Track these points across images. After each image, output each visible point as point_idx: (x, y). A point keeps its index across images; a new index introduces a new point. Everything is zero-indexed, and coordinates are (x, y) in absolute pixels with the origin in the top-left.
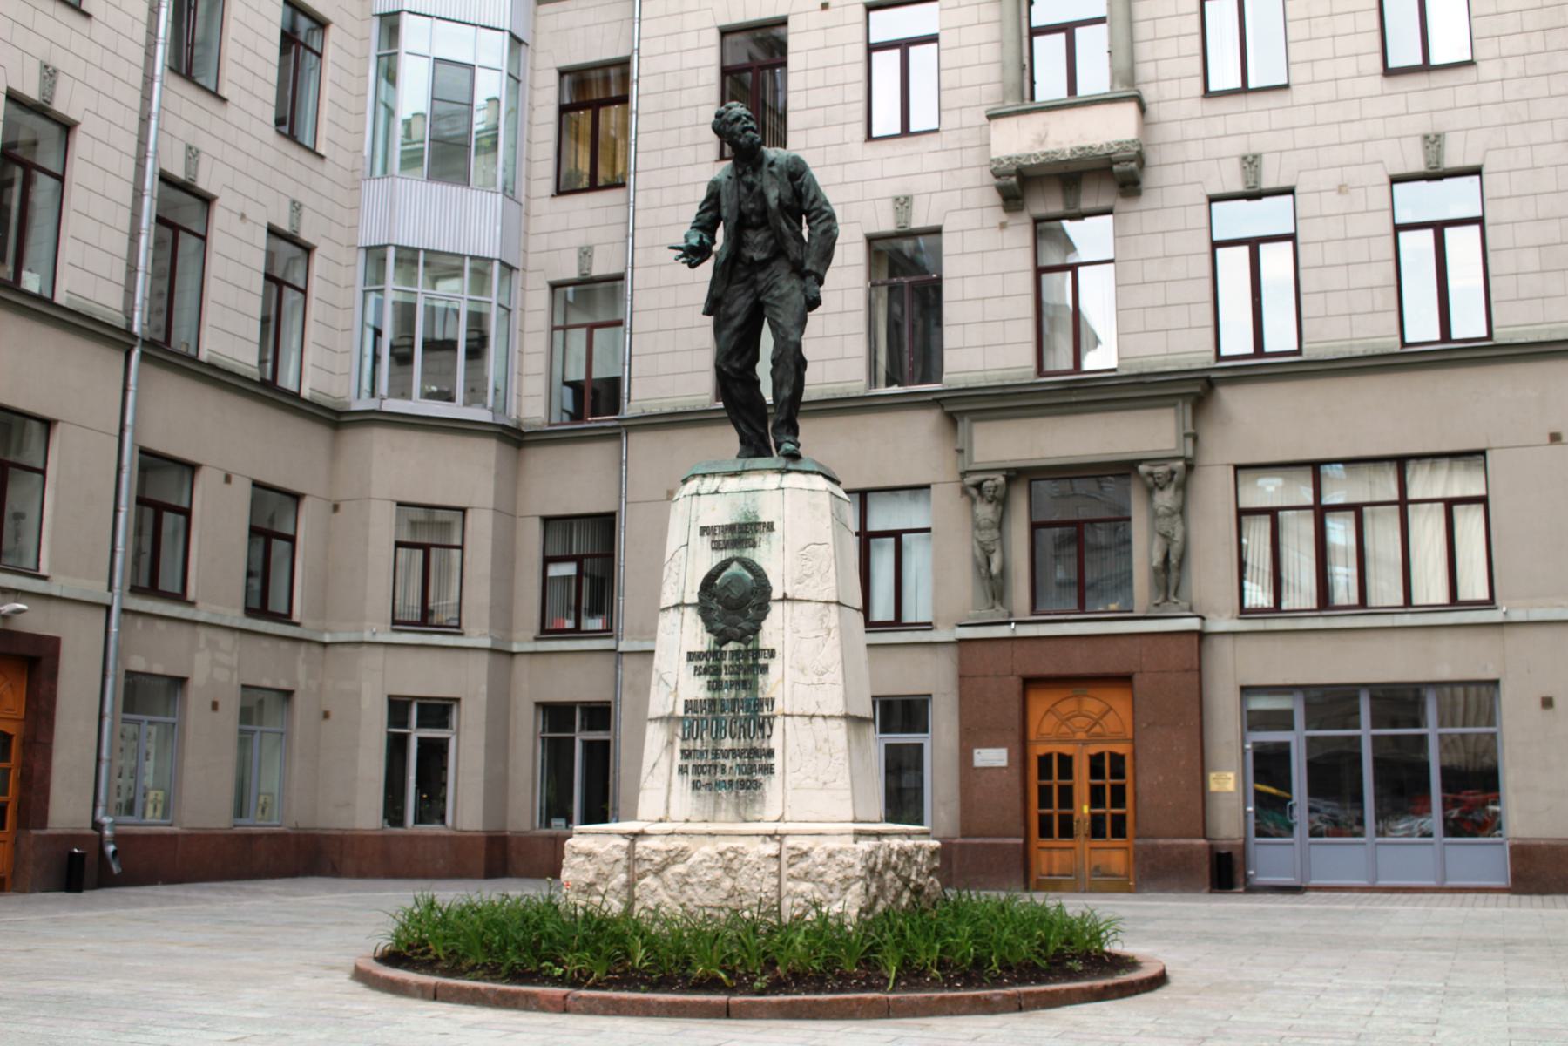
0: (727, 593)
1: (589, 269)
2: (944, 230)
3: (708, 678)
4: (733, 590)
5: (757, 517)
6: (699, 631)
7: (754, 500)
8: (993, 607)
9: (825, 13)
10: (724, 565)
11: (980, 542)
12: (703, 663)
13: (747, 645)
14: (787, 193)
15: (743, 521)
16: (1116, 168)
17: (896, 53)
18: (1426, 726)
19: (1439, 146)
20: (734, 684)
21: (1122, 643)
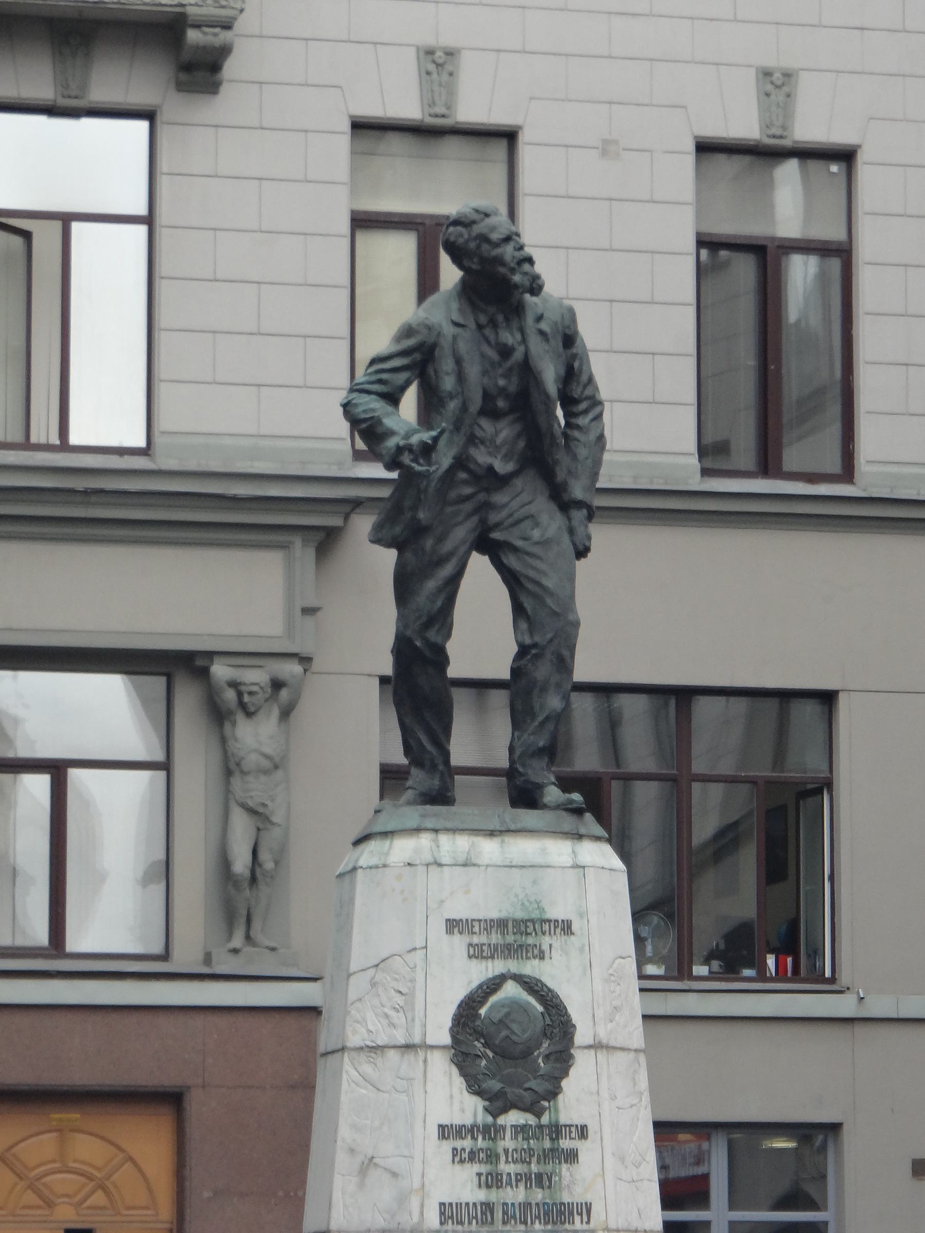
3: (476, 1168)
4: (514, 1027)
5: (543, 910)
6: (456, 1091)
7: (535, 882)
10: (493, 985)
12: (467, 1143)
13: (538, 1115)
15: (519, 915)
16: (192, 36)
18: (825, 1208)
19: (788, 96)
20: (524, 1179)
21: (164, 1022)
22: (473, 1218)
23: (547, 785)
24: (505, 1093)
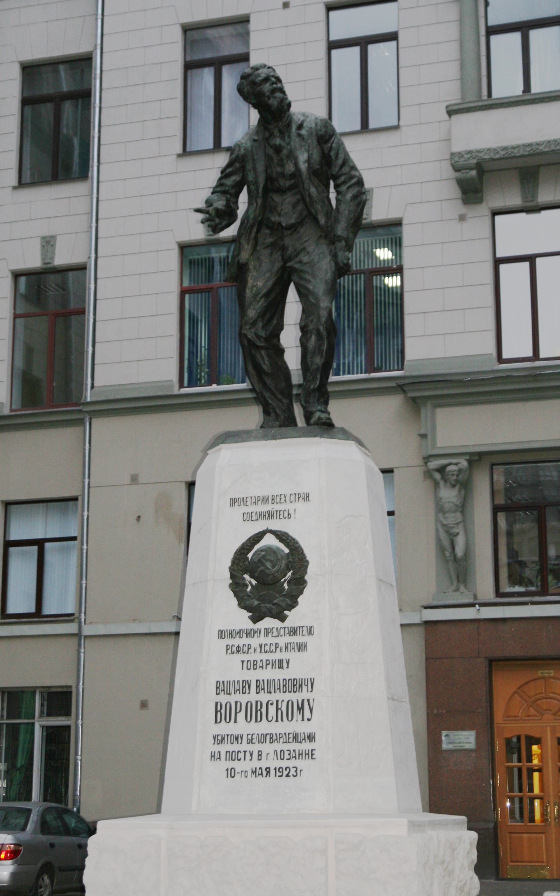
0: (262, 568)
1: (52, 258)
2: (404, 222)
8: (457, 590)
9: (287, 11)
10: (258, 537)
11: (444, 525)
14: (316, 156)
17: (356, 50)
22: (262, 689)
23: (315, 412)
24: (260, 607)
